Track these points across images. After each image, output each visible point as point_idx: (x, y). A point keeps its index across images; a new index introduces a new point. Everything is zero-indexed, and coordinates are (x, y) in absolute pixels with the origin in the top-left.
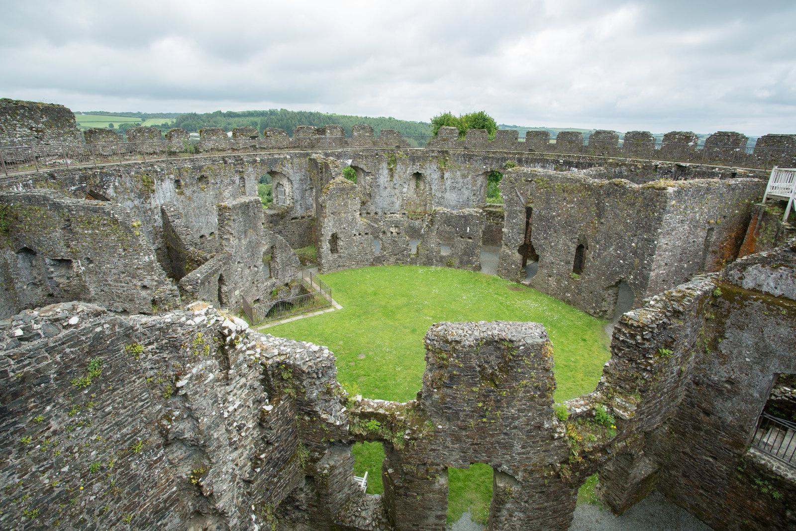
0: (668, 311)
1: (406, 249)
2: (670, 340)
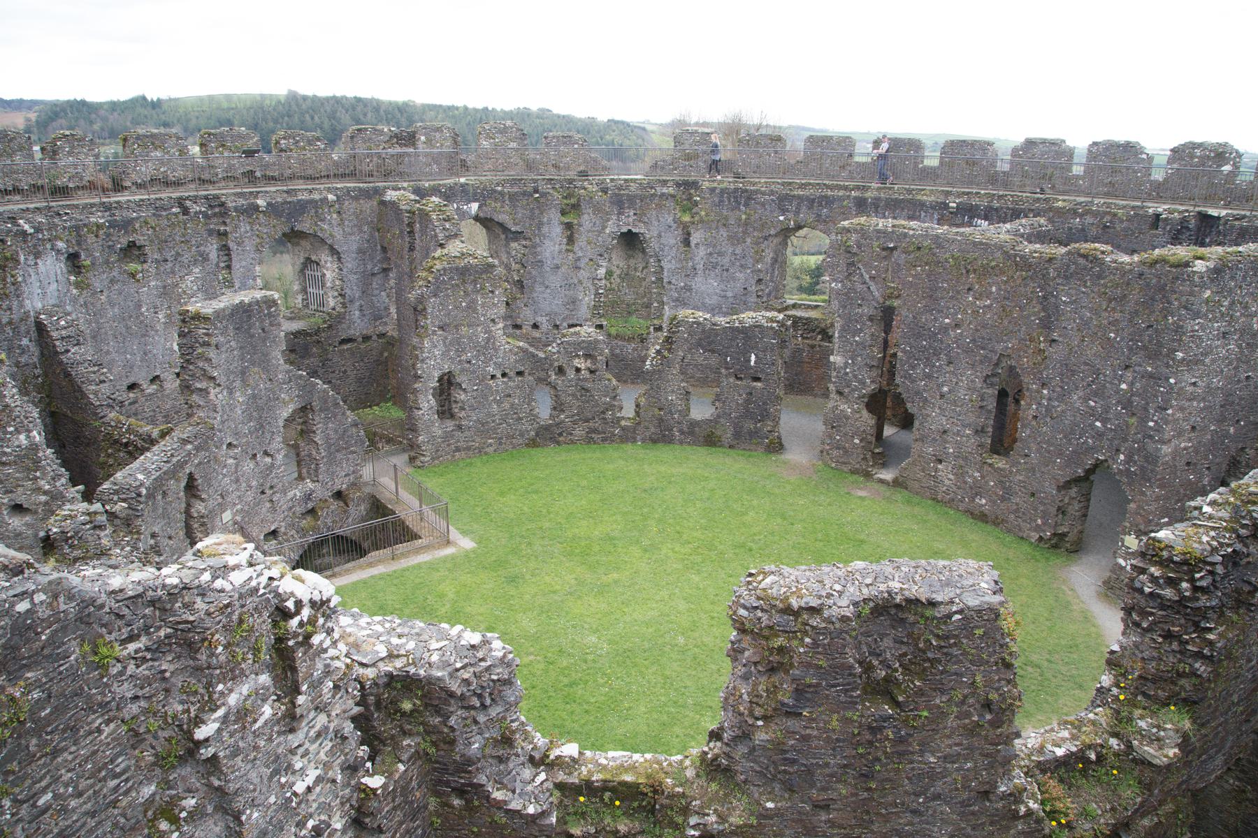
0: (1243, 526)
1: (610, 407)
2: (1246, 588)
